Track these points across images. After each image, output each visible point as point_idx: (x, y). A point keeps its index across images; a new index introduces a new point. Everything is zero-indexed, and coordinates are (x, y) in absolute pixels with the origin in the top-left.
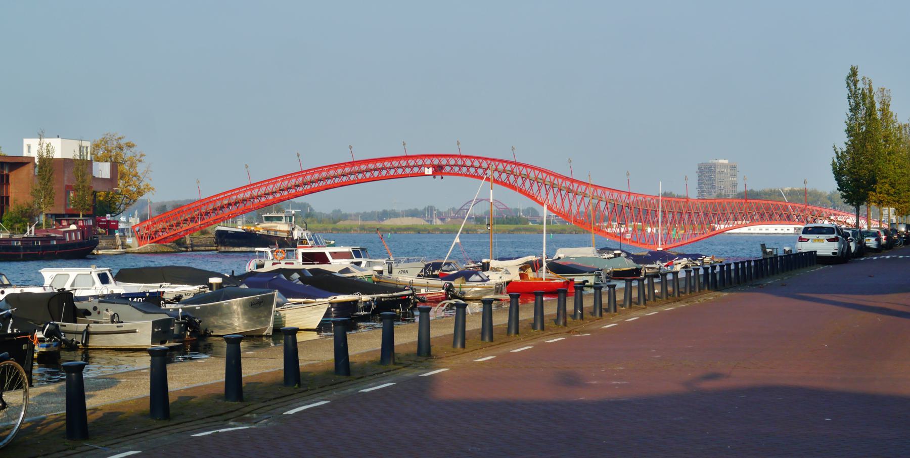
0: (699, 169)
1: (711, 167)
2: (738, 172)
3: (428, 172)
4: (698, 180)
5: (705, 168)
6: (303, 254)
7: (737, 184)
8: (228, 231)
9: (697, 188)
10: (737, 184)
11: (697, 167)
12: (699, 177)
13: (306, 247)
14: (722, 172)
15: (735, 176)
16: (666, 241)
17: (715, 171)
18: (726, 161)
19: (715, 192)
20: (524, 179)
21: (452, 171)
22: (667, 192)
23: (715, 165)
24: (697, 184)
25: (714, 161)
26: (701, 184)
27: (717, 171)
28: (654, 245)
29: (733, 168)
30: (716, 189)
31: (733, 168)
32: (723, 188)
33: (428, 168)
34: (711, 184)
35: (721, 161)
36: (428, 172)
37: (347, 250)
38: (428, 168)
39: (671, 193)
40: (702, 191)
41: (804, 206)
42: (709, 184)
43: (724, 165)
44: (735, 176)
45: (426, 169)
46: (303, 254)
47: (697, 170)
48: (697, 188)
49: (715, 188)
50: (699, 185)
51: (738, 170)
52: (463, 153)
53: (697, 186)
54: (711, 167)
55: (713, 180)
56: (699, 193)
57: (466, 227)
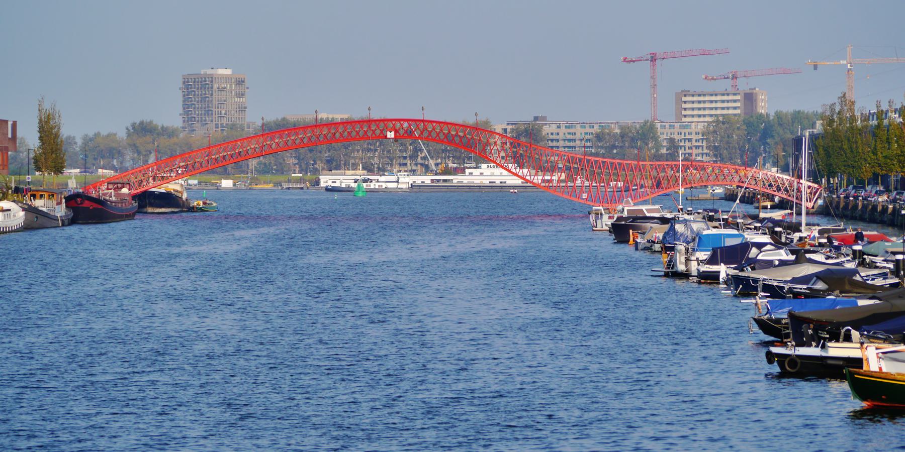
0: (184, 83)
1: (188, 82)
2: (248, 88)
3: (390, 135)
4: (184, 101)
5: (194, 82)
6: (627, 210)
7: (245, 108)
9: (180, 115)
10: (245, 108)
11: (181, 81)
12: (184, 96)
14: (224, 89)
15: (242, 95)
17: (212, 88)
18: (228, 72)
19: (212, 121)
22: (145, 121)
25: (210, 72)
26: (188, 108)
27: (215, 86)
29: (240, 82)
30: (214, 116)
31: (240, 82)
32: (225, 114)
34: (205, 108)
35: (221, 71)
36: (390, 135)
40: (190, 119)
41: (637, 163)
43: (227, 79)
44: (242, 95)
45: (388, 133)
46: (627, 210)
47: (181, 85)
48: (180, 115)
49: (212, 114)
50: (184, 109)
51: (247, 86)
52: (426, 118)
53: (181, 111)
54: (205, 81)
56: (184, 121)
57: (731, 203)
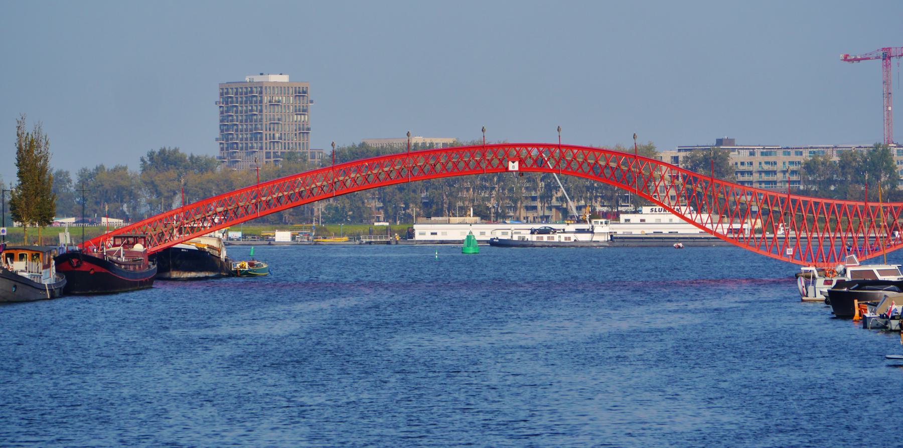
0: (222, 94)
2: (312, 102)
3: (513, 167)
4: (222, 121)
5: (236, 94)
6: (851, 271)
7: (308, 129)
8: (181, 249)
12: (222, 113)
13: (855, 266)
16: (828, 258)
17: (261, 102)
18: (284, 79)
19: (261, 148)
20: (535, 166)
21: (580, 170)
23: (261, 87)
24: (218, 131)
25: (257, 79)
27: (266, 99)
28: (823, 261)
29: (301, 93)
30: (264, 141)
31: (301, 93)
32: (280, 138)
33: (513, 162)
35: (274, 78)
36: (513, 167)
37: (894, 268)
38: (513, 162)
39: (176, 151)
40: (231, 146)
42: (246, 130)
43: (282, 88)
46: (851, 271)
48: (217, 140)
49: (261, 139)
50: (222, 131)
51: (310, 98)
53: (218, 134)
54: (252, 92)
55: (256, 121)
56: (222, 149)
